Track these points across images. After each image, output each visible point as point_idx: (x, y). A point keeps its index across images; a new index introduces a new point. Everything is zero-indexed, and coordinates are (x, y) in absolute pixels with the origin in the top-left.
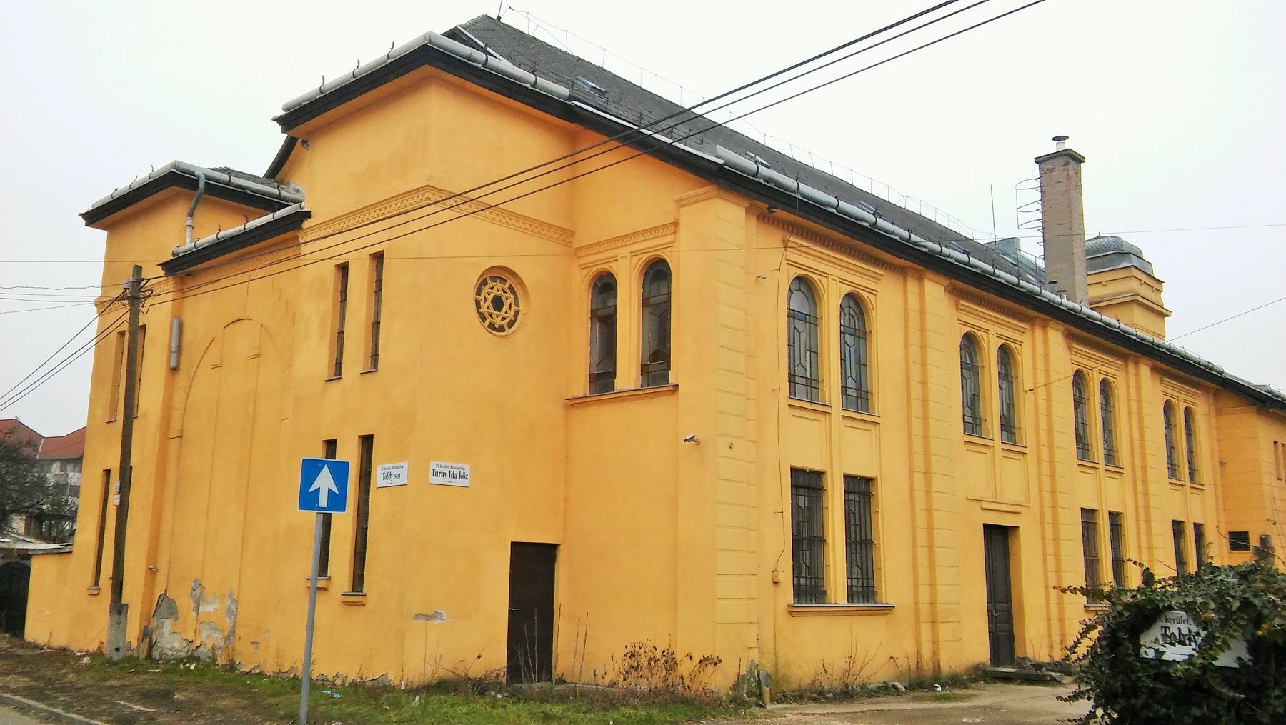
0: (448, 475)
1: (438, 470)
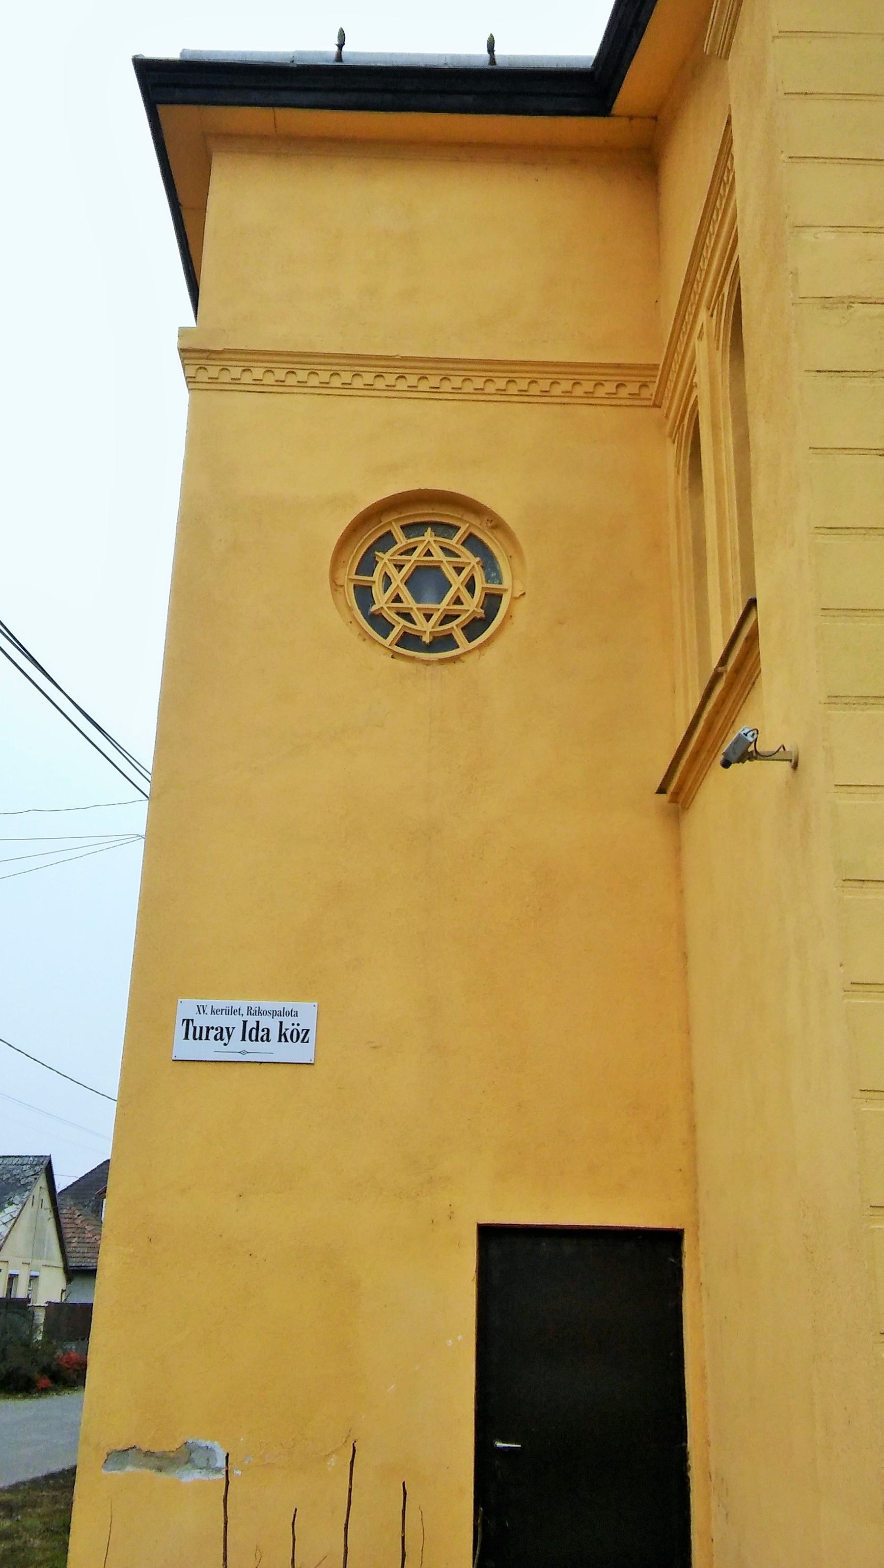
0: (237, 1034)
1: (201, 1021)
